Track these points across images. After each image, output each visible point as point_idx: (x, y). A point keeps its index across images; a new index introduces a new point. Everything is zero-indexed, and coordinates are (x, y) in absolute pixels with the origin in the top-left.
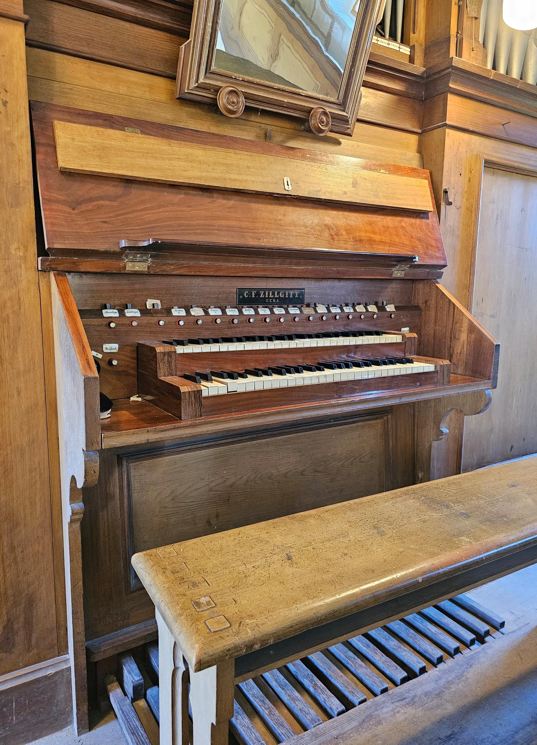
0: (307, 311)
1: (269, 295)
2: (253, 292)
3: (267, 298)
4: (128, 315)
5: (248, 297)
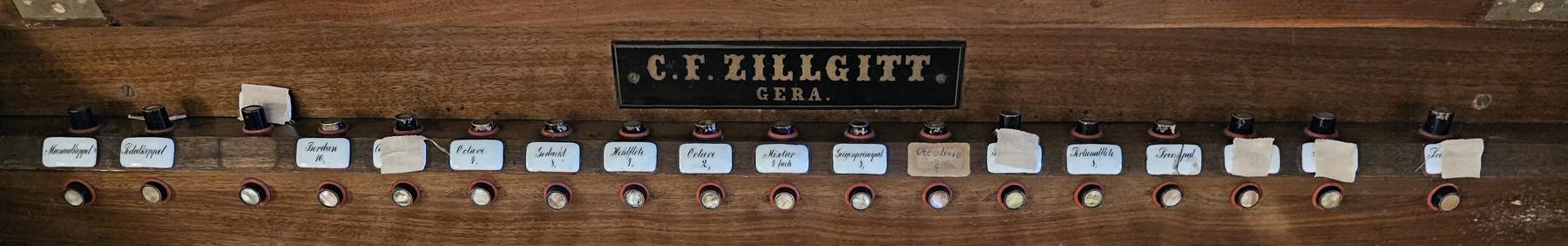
1: (769, 70)
3: (759, 83)
5: (669, 76)
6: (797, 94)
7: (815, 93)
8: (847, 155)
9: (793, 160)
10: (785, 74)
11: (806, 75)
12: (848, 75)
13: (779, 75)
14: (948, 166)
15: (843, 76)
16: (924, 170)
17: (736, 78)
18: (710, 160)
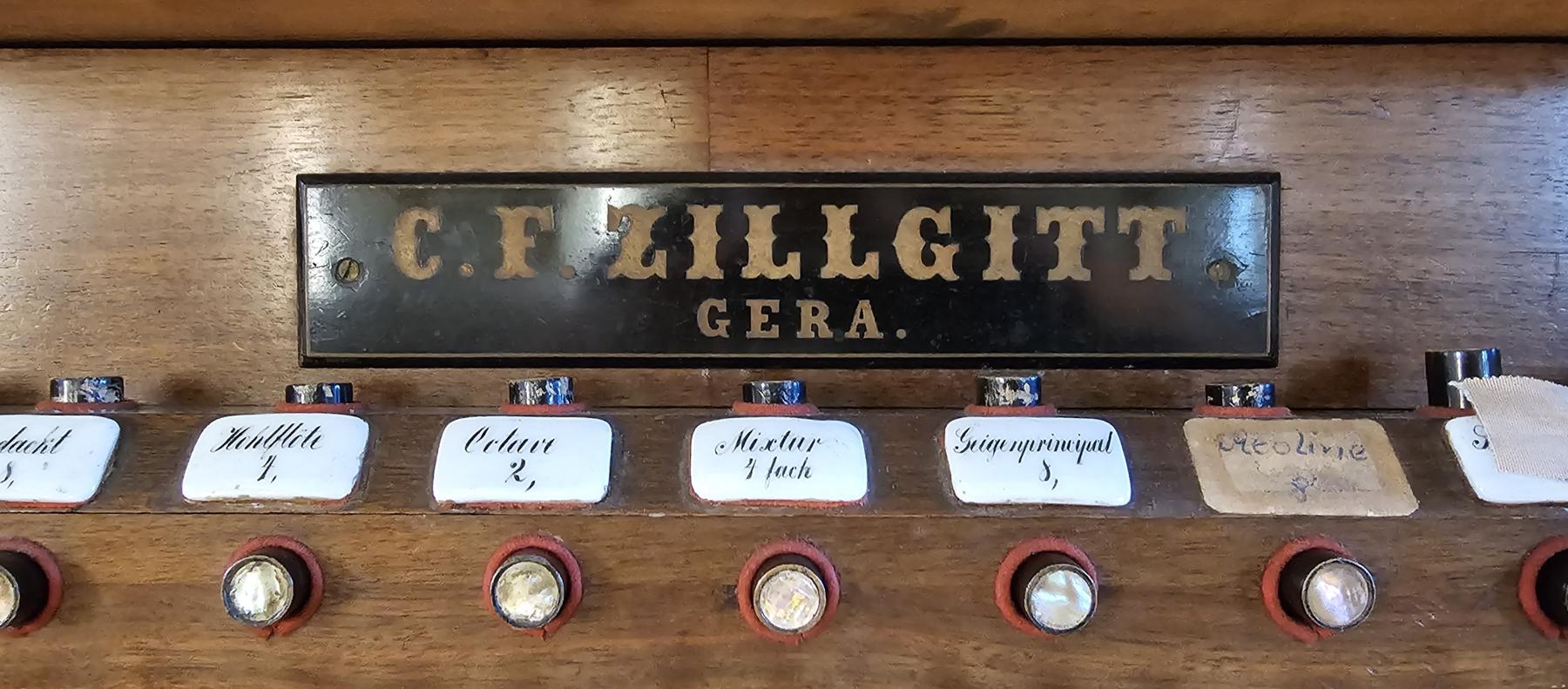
0: (1258, 467)
1: (733, 252)
2: (755, 305)
3: (705, 287)
4: (1222, 495)
5: (450, 267)
6: (813, 318)
7: (866, 315)
8: (994, 445)
9: (816, 459)
10: (779, 260)
11: (839, 262)
12: (957, 264)
13: (760, 262)
14: (1336, 485)
15: (944, 267)
16: (1256, 496)
17: (643, 273)
18: (537, 464)
